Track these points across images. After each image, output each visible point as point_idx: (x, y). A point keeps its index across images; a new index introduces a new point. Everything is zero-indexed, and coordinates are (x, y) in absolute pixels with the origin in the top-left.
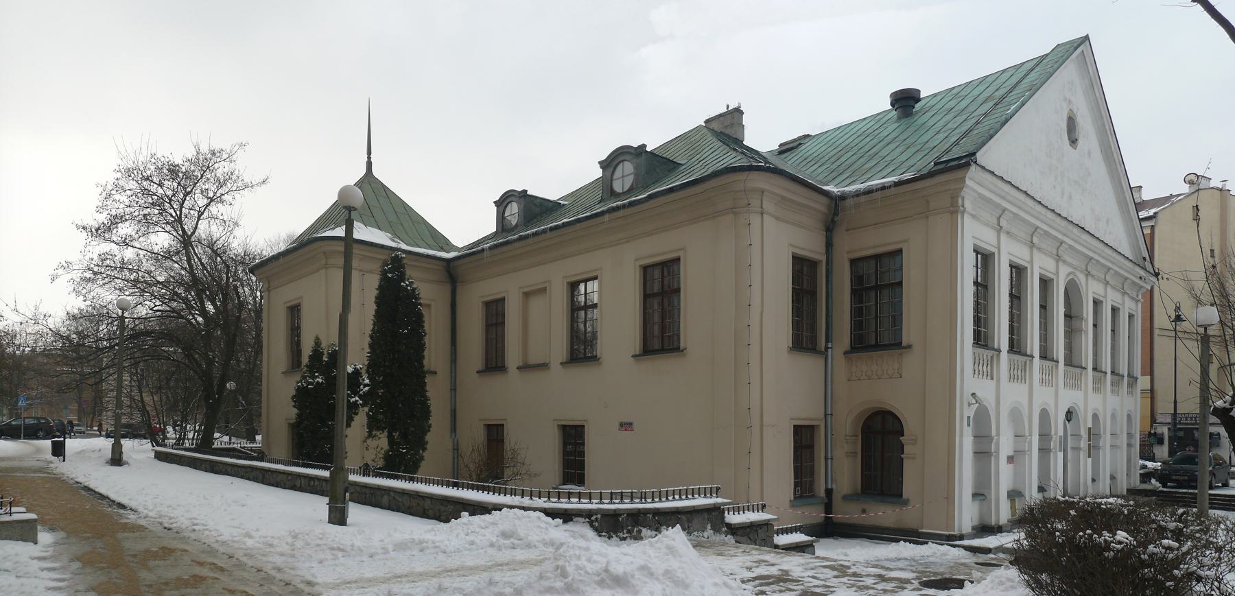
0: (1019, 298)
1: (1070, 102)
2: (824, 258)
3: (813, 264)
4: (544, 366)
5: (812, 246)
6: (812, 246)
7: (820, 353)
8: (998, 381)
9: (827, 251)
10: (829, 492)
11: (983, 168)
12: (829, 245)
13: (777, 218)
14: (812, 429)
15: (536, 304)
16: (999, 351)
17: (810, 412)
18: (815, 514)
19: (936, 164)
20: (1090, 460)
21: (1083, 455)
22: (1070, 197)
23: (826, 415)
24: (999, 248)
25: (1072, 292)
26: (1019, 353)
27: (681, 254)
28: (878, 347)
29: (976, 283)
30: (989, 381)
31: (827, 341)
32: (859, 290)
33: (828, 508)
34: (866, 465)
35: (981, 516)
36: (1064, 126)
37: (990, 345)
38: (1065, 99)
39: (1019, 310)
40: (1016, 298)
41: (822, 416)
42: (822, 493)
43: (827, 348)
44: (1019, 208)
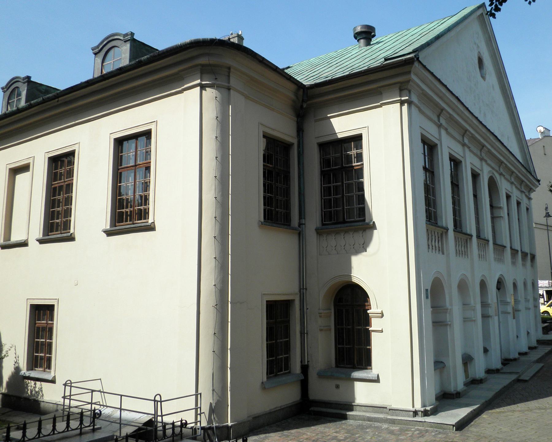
0: (458, 186)
1: (478, 47)
2: (295, 141)
3: (286, 147)
4: (24, 244)
5: (285, 130)
6: (285, 130)
7: (294, 229)
8: (448, 255)
9: (298, 135)
10: (305, 369)
11: (424, 67)
12: (300, 130)
13: (246, 97)
14: (287, 305)
15: (20, 178)
16: (447, 229)
17: (282, 287)
18: (286, 395)
19: (386, 60)
20: (515, 320)
21: (510, 317)
22: (485, 115)
23: (300, 289)
24: (440, 140)
25: (493, 185)
26: (461, 232)
27: (152, 127)
28: (344, 222)
29: (425, 168)
30: (440, 256)
31: (300, 218)
32: (327, 174)
33: (304, 385)
34: (339, 339)
35: (442, 384)
36: (477, 62)
37: (439, 224)
38: (475, 44)
39: (459, 196)
40: (456, 186)
41: (297, 290)
42: (297, 368)
43: (300, 225)
44: (453, 110)
